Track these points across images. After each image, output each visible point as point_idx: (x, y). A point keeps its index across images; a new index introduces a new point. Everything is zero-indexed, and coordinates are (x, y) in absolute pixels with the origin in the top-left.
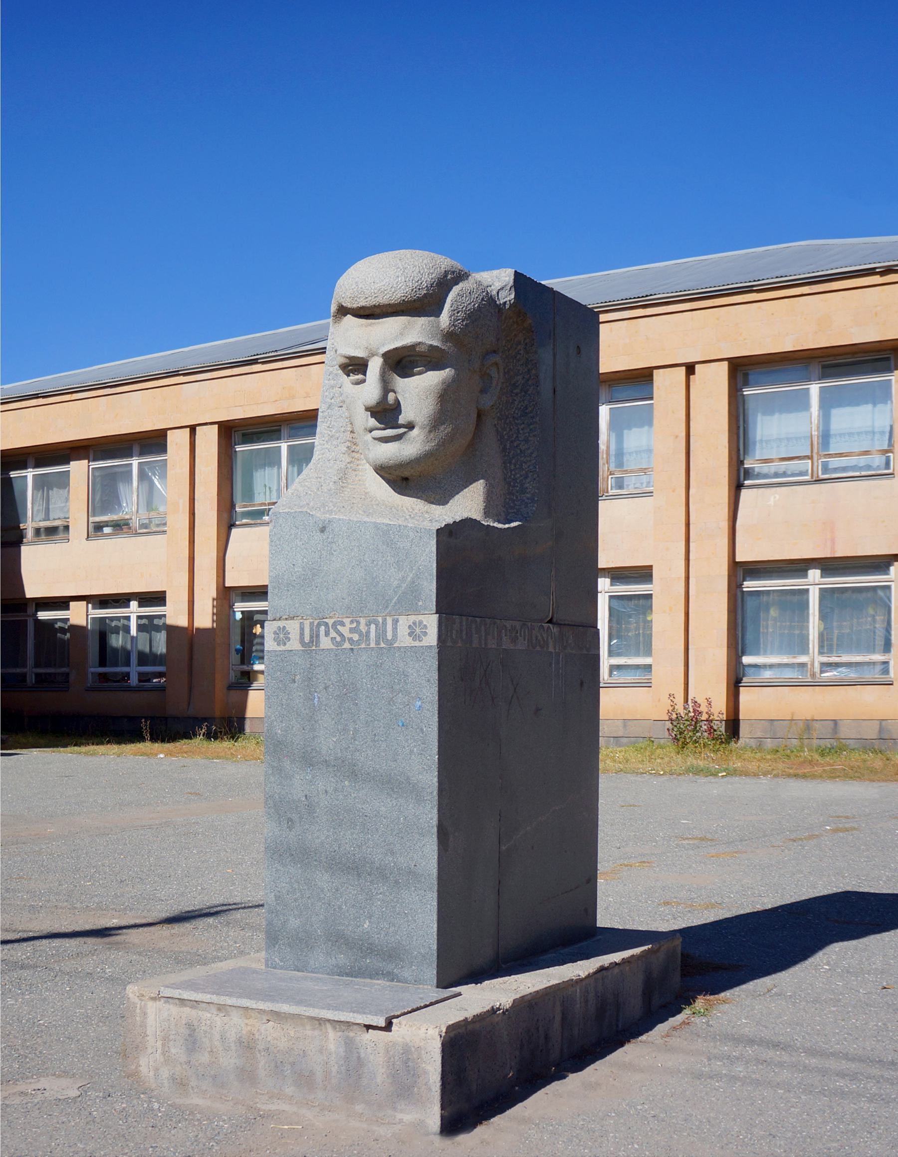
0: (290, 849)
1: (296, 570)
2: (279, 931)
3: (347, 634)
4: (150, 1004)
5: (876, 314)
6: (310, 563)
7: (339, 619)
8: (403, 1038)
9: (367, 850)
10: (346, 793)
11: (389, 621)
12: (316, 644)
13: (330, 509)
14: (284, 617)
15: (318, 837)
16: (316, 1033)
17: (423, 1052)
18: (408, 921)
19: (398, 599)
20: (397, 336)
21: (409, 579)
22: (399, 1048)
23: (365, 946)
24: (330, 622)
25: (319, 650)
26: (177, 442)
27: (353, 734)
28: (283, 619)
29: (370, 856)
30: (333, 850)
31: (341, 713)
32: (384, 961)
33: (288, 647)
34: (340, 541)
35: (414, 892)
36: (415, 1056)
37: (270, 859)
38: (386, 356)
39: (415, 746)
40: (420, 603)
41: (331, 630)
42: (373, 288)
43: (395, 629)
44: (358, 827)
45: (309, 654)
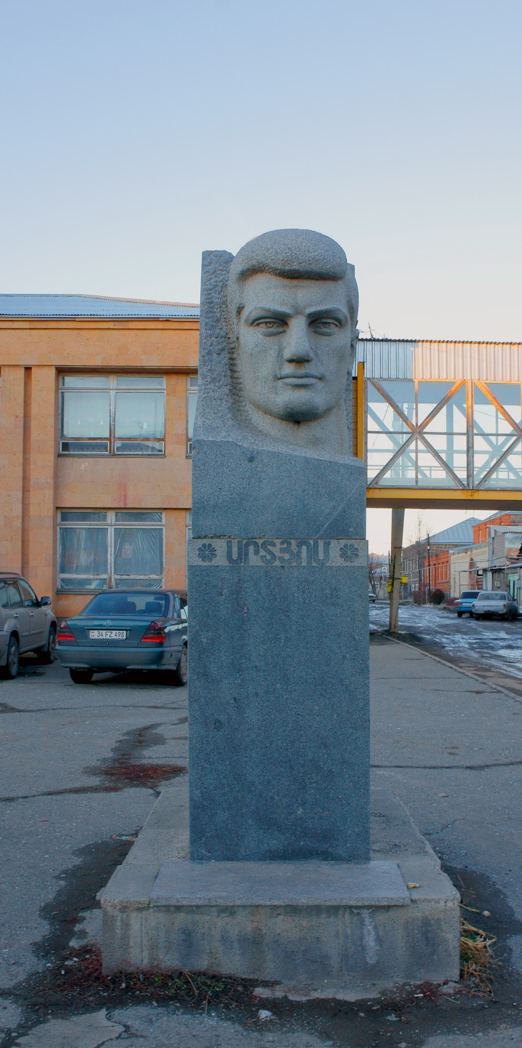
2: (206, 824)
3: (277, 554)
4: (134, 915)
5: (158, 348)
6: (238, 488)
7: (269, 540)
8: (423, 913)
11: (321, 543)
14: (210, 536)
16: (332, 919)
17: (442, 923)
19: (329, 525)
21: (341, 508)
22: (419, 922)
24: (260, 542)
27: (285, 642)
28: (209, 538)
30: (265, 747)
31: (272, 624)
33: (214, 562)
36: (435, 928)
38: (310, 316)
40: (351, 530)
41: (261, 550)
42: (308, 256)
43: (326, 550)
44: (291, 725)
45: (237, 570)
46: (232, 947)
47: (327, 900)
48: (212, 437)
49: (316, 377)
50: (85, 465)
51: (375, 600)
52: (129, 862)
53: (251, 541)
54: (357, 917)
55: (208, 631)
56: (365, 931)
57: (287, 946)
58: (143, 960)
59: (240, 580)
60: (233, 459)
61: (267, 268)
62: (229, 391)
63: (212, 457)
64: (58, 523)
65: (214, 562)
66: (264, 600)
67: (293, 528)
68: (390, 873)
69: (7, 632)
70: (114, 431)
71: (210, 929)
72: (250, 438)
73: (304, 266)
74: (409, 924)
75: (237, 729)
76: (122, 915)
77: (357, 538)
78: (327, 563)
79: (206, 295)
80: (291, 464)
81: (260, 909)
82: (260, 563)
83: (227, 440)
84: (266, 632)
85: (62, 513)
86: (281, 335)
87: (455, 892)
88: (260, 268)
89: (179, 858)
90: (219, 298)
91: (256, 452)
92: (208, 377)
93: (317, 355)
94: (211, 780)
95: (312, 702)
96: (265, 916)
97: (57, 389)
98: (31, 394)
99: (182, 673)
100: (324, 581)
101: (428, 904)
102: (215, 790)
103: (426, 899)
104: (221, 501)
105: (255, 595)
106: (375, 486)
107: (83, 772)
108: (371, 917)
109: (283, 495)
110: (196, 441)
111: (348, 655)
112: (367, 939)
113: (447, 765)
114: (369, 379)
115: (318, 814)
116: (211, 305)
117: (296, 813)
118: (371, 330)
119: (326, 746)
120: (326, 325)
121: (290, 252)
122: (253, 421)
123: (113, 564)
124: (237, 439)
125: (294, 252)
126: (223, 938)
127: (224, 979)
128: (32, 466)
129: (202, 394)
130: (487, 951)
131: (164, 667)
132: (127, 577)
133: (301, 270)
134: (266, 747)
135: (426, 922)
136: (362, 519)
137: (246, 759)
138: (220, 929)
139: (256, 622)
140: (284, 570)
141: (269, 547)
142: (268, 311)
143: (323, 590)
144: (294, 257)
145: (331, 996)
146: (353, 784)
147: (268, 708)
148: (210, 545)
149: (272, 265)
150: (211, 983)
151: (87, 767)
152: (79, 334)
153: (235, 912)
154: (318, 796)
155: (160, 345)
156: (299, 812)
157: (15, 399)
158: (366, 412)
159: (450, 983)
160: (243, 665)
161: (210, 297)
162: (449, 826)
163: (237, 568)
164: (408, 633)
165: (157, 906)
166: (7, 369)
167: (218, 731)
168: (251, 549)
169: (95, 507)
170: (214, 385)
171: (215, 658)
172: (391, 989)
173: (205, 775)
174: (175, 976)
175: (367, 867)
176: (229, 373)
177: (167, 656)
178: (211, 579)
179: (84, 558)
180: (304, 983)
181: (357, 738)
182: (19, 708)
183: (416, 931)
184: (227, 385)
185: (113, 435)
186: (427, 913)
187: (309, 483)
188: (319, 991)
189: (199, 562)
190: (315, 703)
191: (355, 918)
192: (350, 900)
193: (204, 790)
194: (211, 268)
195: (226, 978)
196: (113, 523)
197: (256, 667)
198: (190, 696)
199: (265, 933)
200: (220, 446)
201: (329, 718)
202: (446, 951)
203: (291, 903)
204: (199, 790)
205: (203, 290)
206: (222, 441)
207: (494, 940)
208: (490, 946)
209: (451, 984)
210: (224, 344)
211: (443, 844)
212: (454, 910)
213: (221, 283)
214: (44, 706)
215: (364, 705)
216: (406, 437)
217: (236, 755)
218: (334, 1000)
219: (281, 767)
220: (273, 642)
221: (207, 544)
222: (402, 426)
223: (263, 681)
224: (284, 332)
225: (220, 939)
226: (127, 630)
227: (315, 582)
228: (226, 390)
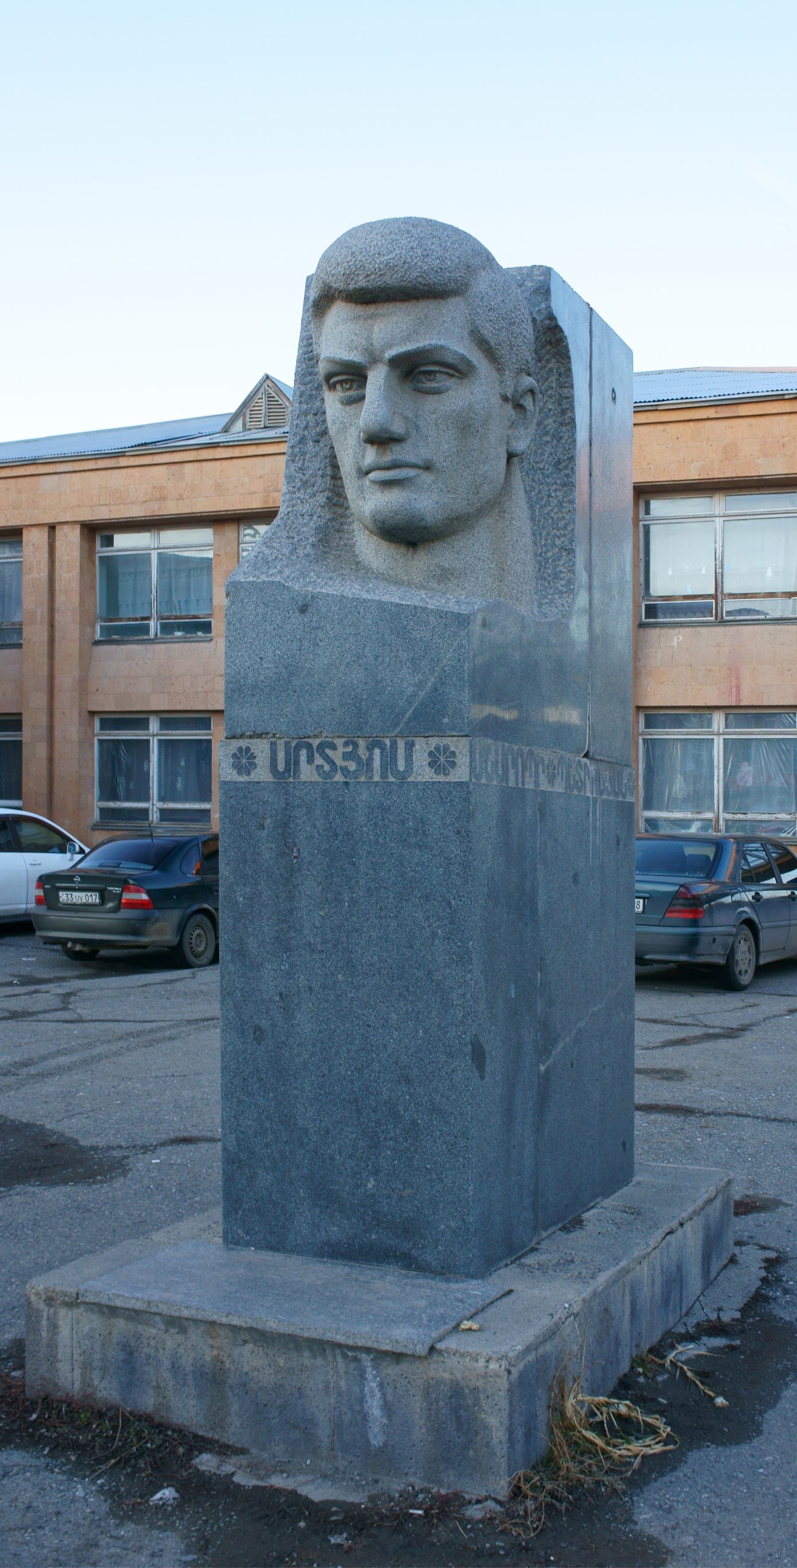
0: (258, 1071)
1: (265, 666)
2: (243, 1190)
3: (339, 762)
4: (63, 1312)
5: (784, 445)
8: (451, 1373)
9: (370, 1076)
10: (339, 992)
11: (401, 744)
12: (294, 774)
13: (312, 580)
14: (248, 734)
15: (299, 1055)
16: (319, 1361)
17: (482, 1396)
18: (431, 1180)
19: (413, 713)
20: (409, 335)
21: (430, 684)
22: (446, 1389)
23: (368, 1215)
24: (315, 742)
25: (299, 783)
26: (34, 539)
27: (349, 906)
28: (247, 737)
29: (375, 1085)
30: (321, 1074)
31: (332, 875)
32: (397, 1237)
33: (254, 777)
34: (328, 625)
35: (439, 1138)
36: (470, 1402)
37: (230, 1085)
38: (395, 362)
39: (439, 927)
40: (446, 720)
41: (316, 755)
43: (409, 757)
44: (357, 1042)
45: (283, 788)
50: (678, 638)
55: (245, 885)
56: (366, 1389)
64: (640, 731)
67: (362, 720)
70: (722, 582)
71: (157, 1350)
73: (374, 280)
74: (431, 1390)
75: (283, 1043)
77: (454, 734)
79: (305, 346)
82: (316, 778)
85: (646, 715)
92: (297, 480)
93: (417, 428)
95: (388, 1007)
97: (636, 520)
99: (737, 971)
101: (459, 1359)
102: (256, 1136)
104: (262, 678)
108: (375, 1368)
112: (370, 1403)
116: (312, 362)
119: (408, 1081)
120: (430, 375)
123: (721, 796)
131: (701, 960)
132: (742, 817)
134: (324, 1076)
135: (457, 1391)
137: (296, 1092)
143: (403, 822)
148: (248, 749)
152: (664, 430)
154: (396, 1162)
155: (786, 439)
156: (370, 1186)
167: (259, 1044)
168: (303, 754)
169: (692, 704)
171: (255, 929)
177: (704, 941)
179: (679, 786)
181: (453, 1071)
183: (441, 1403)
184: (324, 491)
185: (719, 590)
186: (459, 1376)
187: (384, 644)
188: (285, 1475)
191: (353, 1365)
193: (241, 1136)
195: (174, 1431)
196: (721, 731)
197: (310, 945)
198: (222, 986)
200: (261, 590)
202: (488, 1445)
203: (255, 1325)
206: (264, 582)
212: (500, 1377)
217: (283, 1085)
218: (294, 1493)
219: (344, 1109)
220: (333, 905)
226: (644, 898)
227: (392, 809)
228: (321, 499)
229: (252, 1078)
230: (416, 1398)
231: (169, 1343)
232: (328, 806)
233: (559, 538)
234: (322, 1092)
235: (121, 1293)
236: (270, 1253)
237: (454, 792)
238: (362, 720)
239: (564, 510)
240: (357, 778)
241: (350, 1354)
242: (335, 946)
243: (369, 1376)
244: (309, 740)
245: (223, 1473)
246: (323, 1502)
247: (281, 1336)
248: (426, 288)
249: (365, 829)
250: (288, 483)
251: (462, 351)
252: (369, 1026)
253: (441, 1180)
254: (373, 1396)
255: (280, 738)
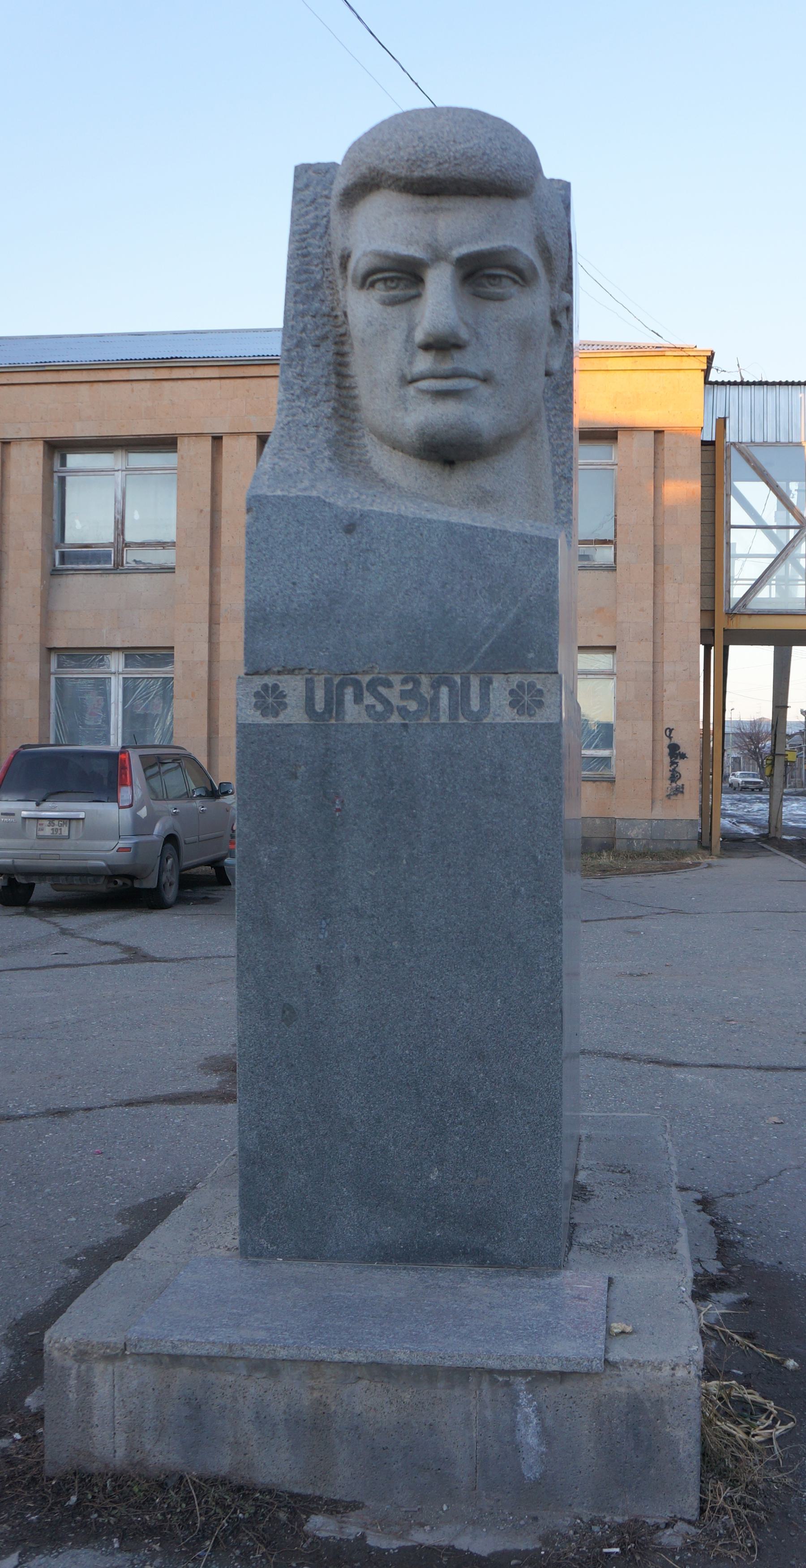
1: (299, 592)
3: (396, 701)
4: (99, 1368)
6: (326, 582)
11: (475, 683)
12: (337, 714)
14: (276, 669)
16: (457, 1392)
21: (511, 615)
24: (365, 679)
28: (274, 673)
30: (371, 1055)
33: (282, 718)
35: (521, 1118)
36: (652, 1416)
37: (250, 1074)
40: (531, 655)
41: (366, 694)
42: (453, 149)
43: (485, 696)
44: (417, 1017)
46: (274, 1434)
47: (446, 1356)
48: (282, 490)
49: (474, 377)
51: (762, 788)
52: (138, 1255)
53: (349, 680)
54: (505, 1389)
55: (271, 843)
56: (519, 1416)
57: (375, 1437)
58: (115, 1451)
59: (328, 750)
60: (318, 528)
61: (384, 178)
62: (332, 411)
63: (281, 525)
65: (282, 718)
66: (370, 787)
67: (425, 654)
68: (585, 1300)
69: (157, 836)
71: (235, 1399)
72: (351, 490)
73: (447, 169)
76: (79, 1367)
77: (541, 670)
78: (485, 717)
79: (297, 241)
80: (421, 535)
81: (322, 1366)
82: (365, 719)
83: (306, 494)
84: (375, 846)
86: (412, 301)
87: (695, 1348)
88: (373, 179)
89: (229, 1249)
90: (320, 247)
91: (358, 515)
92: (296, 387)
93: (477, 335)
94: (275, 1113)
95: (457, 975)
96: (333, 1380)
98: (221, 477)
100: (480, 751)
102: (284, 1131)
103: (635, 1361)
104: (295, 605)
105: (355, 777)
106: (742, 610)
107: (202, 1067)
108: (530, 1391)
109: (407, 592)
110: (253, 497)
111: (523, 889)
112: (523, 1432)
113: (797, 1064)
114: (734, 444)
115: (468, 1180)
116: (306, 259)
117: (429, 1177)
118: (740, 370)
121: (421, 145)
122: (372, 464)
124: (327, 492)
125: (429, 144)
126: (258, 1417)
127: (258, 1495)
128: (223, 586)
129: (283, 417)
130: (771, 1451)
133: (441, 176)
134: (374, 1057)
136: (551, 636)
138: (254, 1401)
139: (355, 827)
140: (407, 731)
141: (381, 689)
142: (385, 256)
144: (428, 152)
145: (445, 1542)
146: (530, 1128)
147: (378, 986)
148: (275, 687)
149: (391, 171)
150: (233, 1500)
151: (211, 1057)
153: (278, 1371)
154: (466, 1149)
157: (198, 485)
158: (728, 496)
159: (679, 1523)
160: (333, 906)
161: (304, 245)
162: (771, 1180)
163: (323, 728)
164: (799, 838)
165: (138, 1354)
166: (186, 439)
170: (306, 401)
172: (563, 1531)
173: (266, 1104)
174: (171, 1484)
175: (549, 1284)
176: (333, 379)
178: (277, 748)
180: (404, 1509)
181: (539, 1043)
182: (151, 953)
184: (328, 401)
186: (638, 1388)
187: (453, 570)
188: (427, 1528)
189: (255, 717)
190: (463, 978)
192: (489, 1358)
194: (308, 194)
197: (356, 909)
199: (335, 1412)
200: (294, 506)
201: (488, 1005)
203: (378, 1359)
204: (256, 1132)
205: (293, 233)
206: (298, 497)
207: (791, 1425)
208: (778, 1438)
209: (681, 1526)
210: (327, 328)
211: (752, 1215)
213: (325, 219)
214: (193, 953)
215: (552, 982)
216: (792, 533)
217: (320, 1071)
218: (451, 1550)
220: (387, 863)
221: (270, 685)
222: (788, 517)
223: (368, 935)
224: (418, 296)
225: (253, 1419)
229: (280, 1064)
230: (583, 1419)
231: (252, 1390)
232: (381, 751)
233: (558, 465)
234: (372, 1076)
235: (189, 1337)
236: (307, 1264)
237: (542, 735)
238: (425, 654)
239: (563, 437)
240: (418, 719)
241: (501, 1379)
242: (389, 909)
243: (523, 1401)
244: (356, 676)
245: (351, 1538)
246: (493, 1555)
247: (411, 1367)
248: (503, 184)
249: (428, 776)
250: (285, 390)
251: (531, 257)
252: (433, 998)
253: (523, 1164)
254: (527, 1423)
255: (318, 674)
